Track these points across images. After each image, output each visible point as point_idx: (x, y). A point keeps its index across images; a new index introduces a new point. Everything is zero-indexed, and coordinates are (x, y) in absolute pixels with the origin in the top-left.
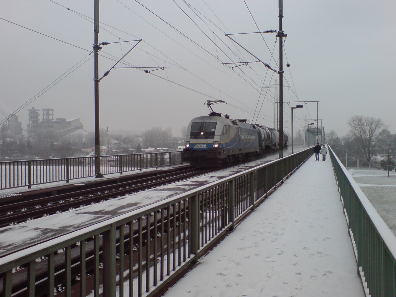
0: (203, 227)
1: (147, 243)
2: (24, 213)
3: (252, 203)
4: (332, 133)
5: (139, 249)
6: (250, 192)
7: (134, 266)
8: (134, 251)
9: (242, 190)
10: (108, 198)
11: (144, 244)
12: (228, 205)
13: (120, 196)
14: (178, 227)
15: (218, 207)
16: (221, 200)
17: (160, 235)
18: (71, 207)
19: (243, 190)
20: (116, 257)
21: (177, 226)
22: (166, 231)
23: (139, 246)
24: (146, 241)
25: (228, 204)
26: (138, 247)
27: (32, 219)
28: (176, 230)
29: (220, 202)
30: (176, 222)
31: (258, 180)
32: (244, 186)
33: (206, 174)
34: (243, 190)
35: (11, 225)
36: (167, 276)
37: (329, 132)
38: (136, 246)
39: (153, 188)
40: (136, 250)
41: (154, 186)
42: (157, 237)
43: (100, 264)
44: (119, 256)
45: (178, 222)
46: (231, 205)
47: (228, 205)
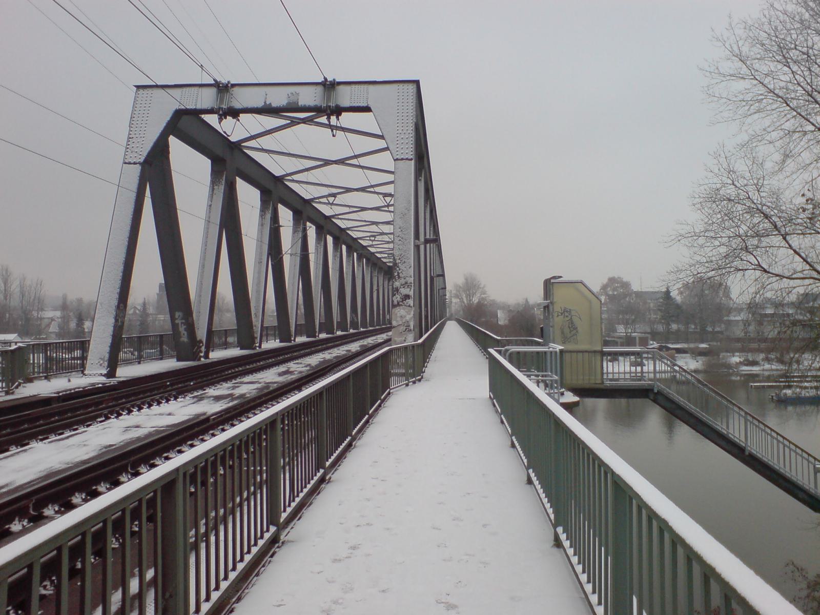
0: (286, 464)
1: (82, 571)
2: (92, 413)
3: (273, 518)
4: (470, 286)
5: (123, 546)
6: (265, 475)
7: (191, 531)
8: (113, 549)
9: (299, 423)
10: (6, 447)
11: (74, 573)
12: (265, 468)
13: (17, 447)
14: (193, 497)
15: (246, 468)
16: (254, 448)
17: (52, 588)
18: (12, 444)
19: (216, 480)
20: (40, 591)
21: (133, 534)
22: (204, 483)
23: (124, 539)
24: (79, 565)
25: (267, 467)
26: (121, 540)
27: (38, 441)
28: (211, 488)
29: (252, 452)
30: (132, 523)
31: (300, 421)
32: (254, 443)
33: (229, 382)
34: (301, 425)
35: (31, 443)
36: (207, 603)
37: (461, 281)
38: (117, 539)
39: (70, 431)
40: (117, 546)
41: (40, 437)
42: (38, 598)
43: (45, 583)
44: (138, 526)
45: (137, 523)
46: (340, 416)
47: (267, 470)
